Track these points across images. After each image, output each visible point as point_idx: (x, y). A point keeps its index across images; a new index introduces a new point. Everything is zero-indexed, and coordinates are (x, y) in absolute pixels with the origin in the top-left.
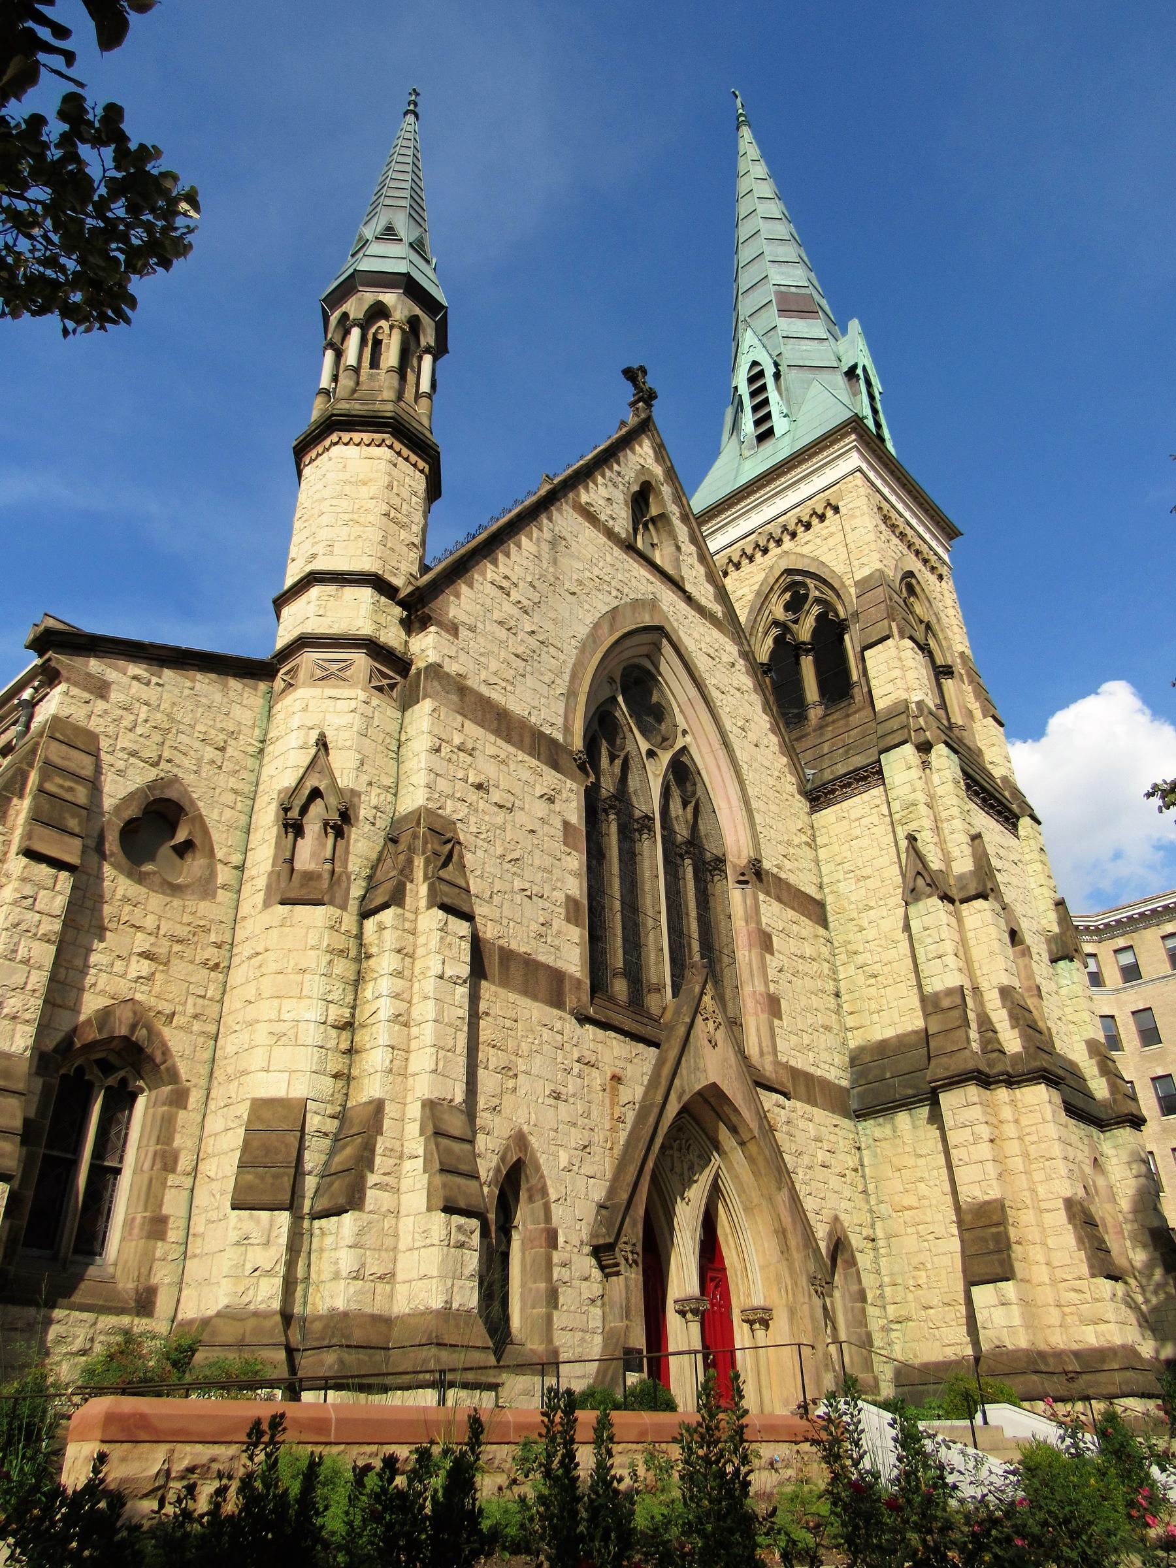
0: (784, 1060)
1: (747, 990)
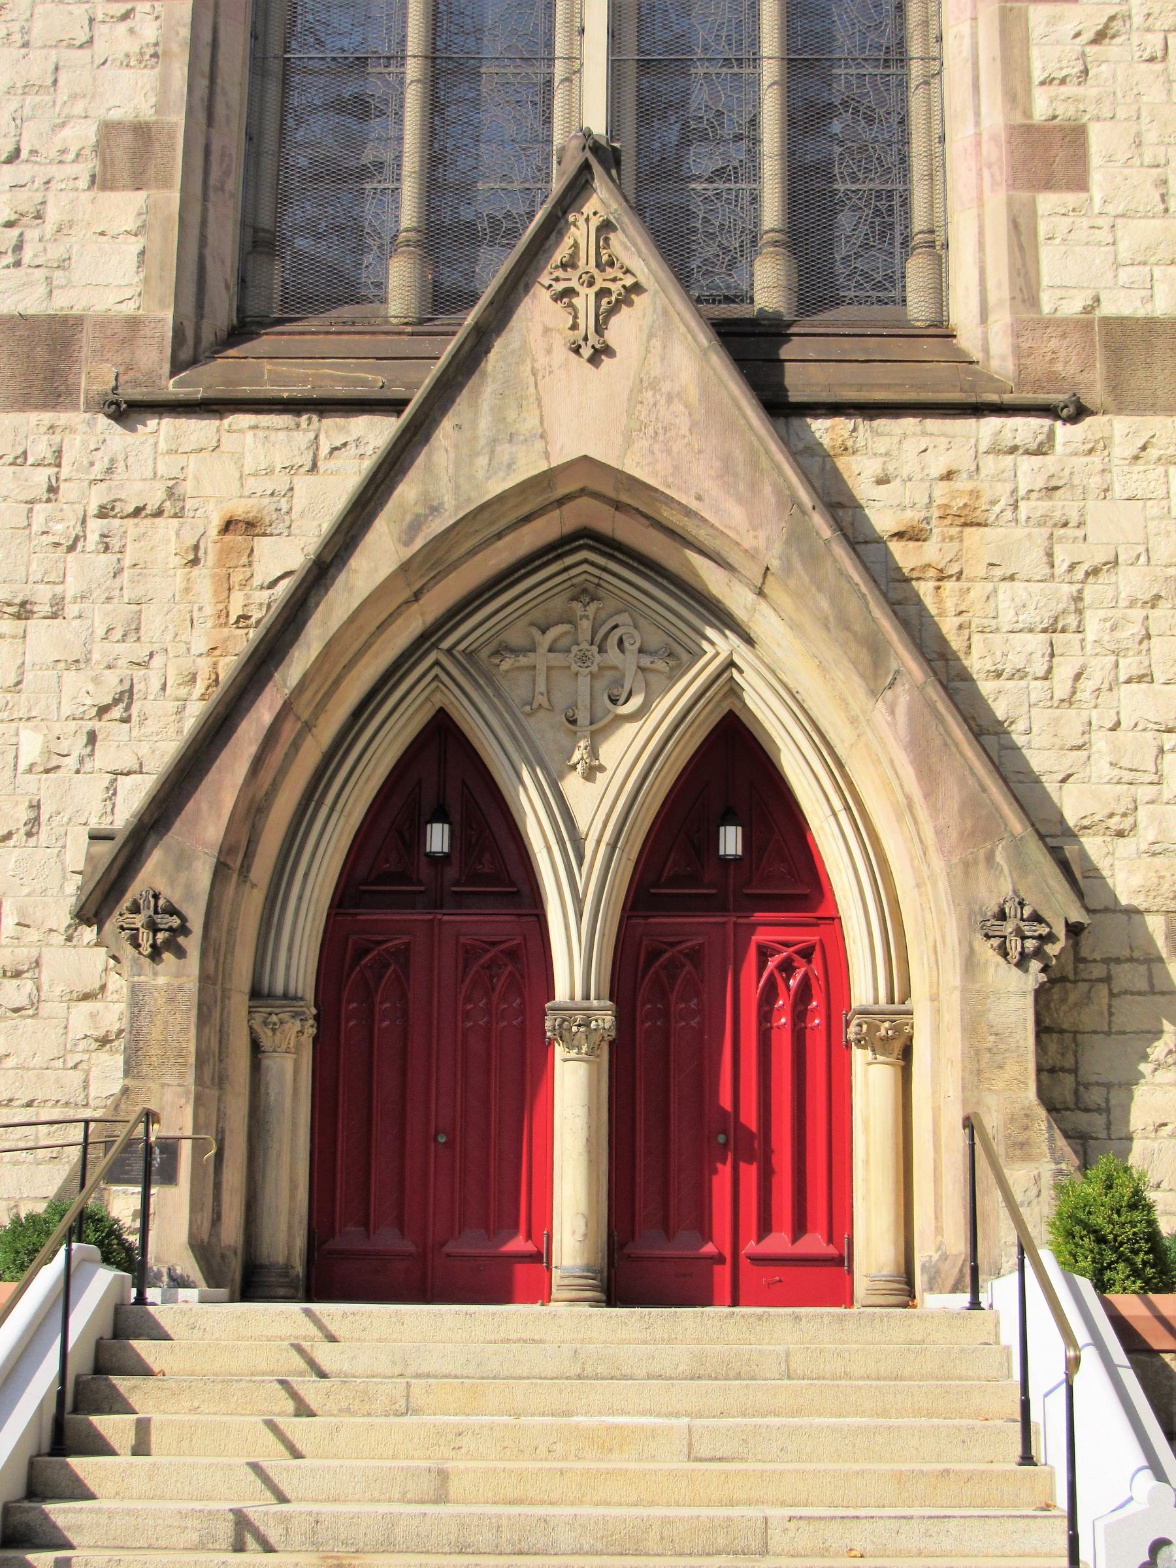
0: (1073, 307)
1: (960, 136)
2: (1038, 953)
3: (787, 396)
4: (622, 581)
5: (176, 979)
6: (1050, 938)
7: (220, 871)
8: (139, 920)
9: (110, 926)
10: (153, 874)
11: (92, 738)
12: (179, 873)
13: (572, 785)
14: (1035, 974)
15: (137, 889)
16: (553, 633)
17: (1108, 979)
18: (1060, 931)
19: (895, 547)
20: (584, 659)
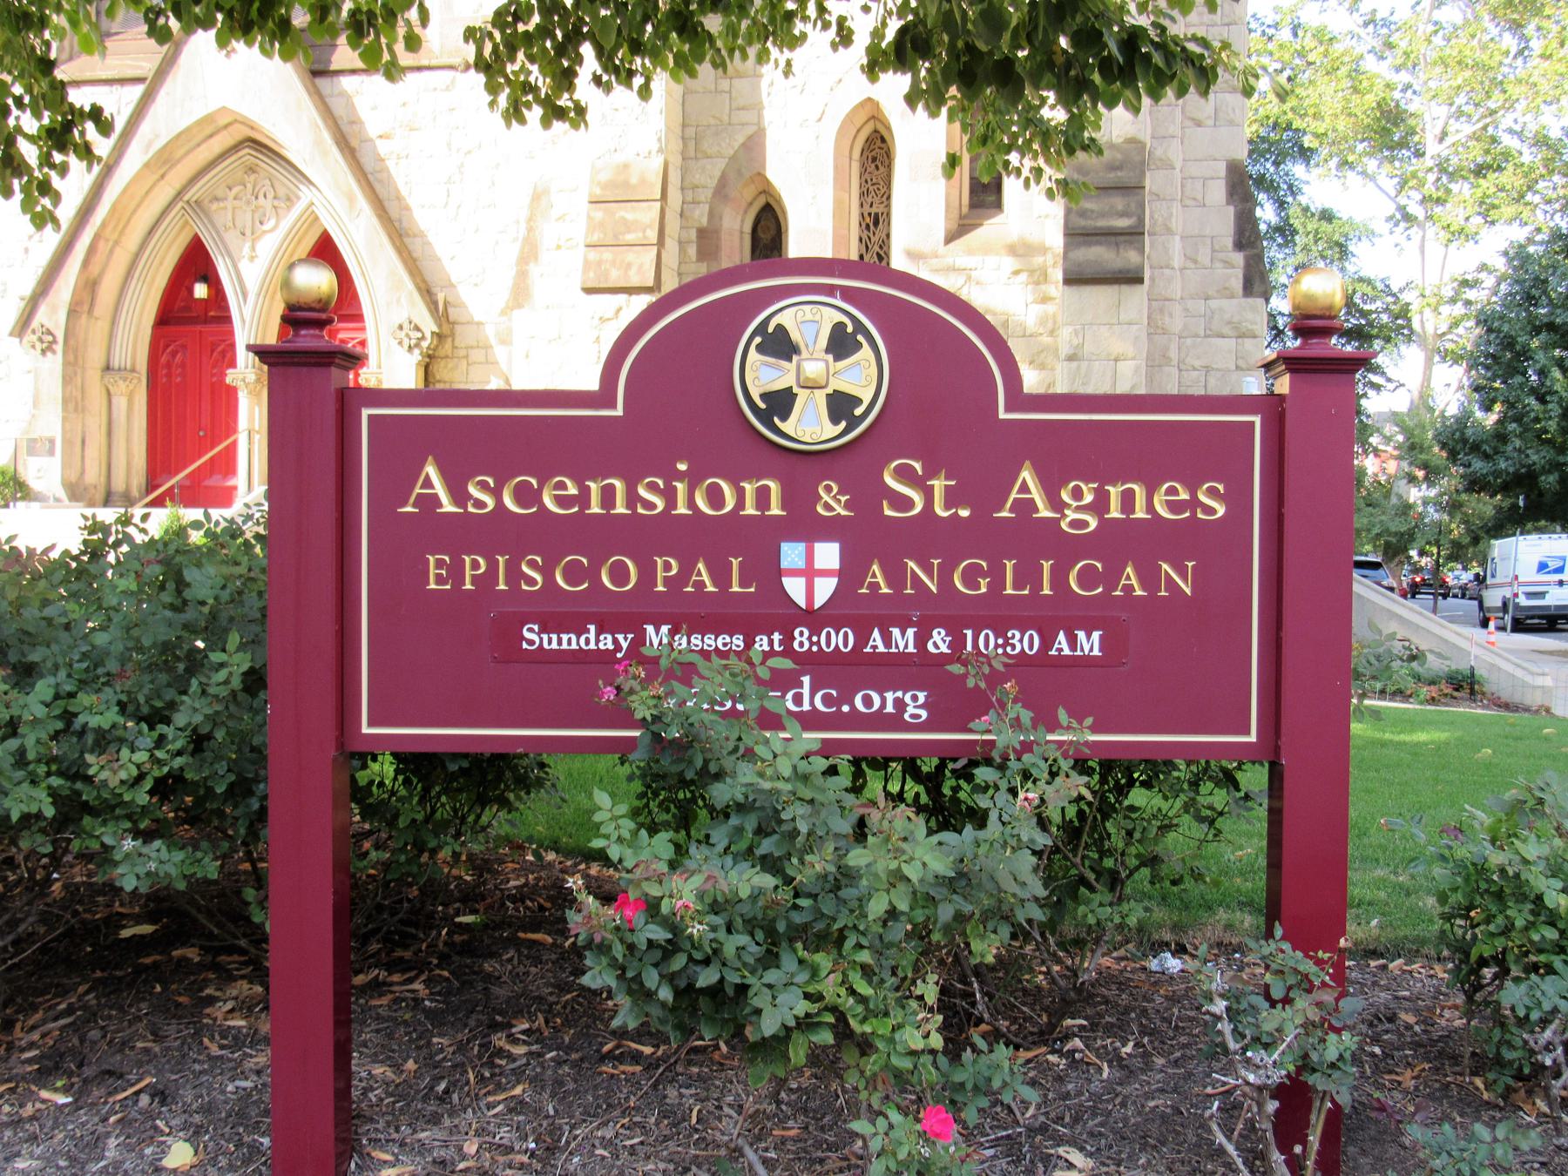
2: (417, 345)
3: (330, 62)
4: (266, 165)
5: (55, 362)
6: (423, 338)
7: (73, 313)
8: (34, 338)
9: (26, 339)
10: (41, 317)
11: (26, 250)
12: (53, 315)
13: (244, 265)
14: (416, 356)
15: (35, 324)
16: (235, 190)
17: (467, 357)
18: (428, 335)
19: (379, 143)
20: (248, 203)
